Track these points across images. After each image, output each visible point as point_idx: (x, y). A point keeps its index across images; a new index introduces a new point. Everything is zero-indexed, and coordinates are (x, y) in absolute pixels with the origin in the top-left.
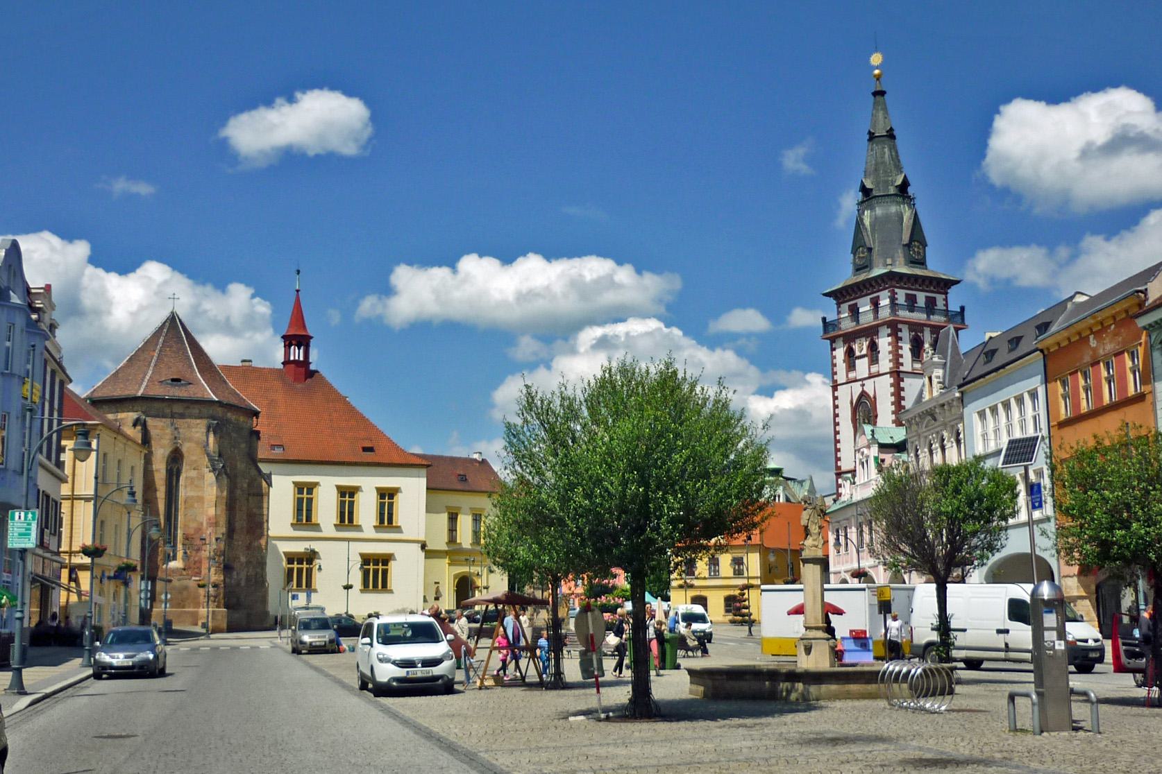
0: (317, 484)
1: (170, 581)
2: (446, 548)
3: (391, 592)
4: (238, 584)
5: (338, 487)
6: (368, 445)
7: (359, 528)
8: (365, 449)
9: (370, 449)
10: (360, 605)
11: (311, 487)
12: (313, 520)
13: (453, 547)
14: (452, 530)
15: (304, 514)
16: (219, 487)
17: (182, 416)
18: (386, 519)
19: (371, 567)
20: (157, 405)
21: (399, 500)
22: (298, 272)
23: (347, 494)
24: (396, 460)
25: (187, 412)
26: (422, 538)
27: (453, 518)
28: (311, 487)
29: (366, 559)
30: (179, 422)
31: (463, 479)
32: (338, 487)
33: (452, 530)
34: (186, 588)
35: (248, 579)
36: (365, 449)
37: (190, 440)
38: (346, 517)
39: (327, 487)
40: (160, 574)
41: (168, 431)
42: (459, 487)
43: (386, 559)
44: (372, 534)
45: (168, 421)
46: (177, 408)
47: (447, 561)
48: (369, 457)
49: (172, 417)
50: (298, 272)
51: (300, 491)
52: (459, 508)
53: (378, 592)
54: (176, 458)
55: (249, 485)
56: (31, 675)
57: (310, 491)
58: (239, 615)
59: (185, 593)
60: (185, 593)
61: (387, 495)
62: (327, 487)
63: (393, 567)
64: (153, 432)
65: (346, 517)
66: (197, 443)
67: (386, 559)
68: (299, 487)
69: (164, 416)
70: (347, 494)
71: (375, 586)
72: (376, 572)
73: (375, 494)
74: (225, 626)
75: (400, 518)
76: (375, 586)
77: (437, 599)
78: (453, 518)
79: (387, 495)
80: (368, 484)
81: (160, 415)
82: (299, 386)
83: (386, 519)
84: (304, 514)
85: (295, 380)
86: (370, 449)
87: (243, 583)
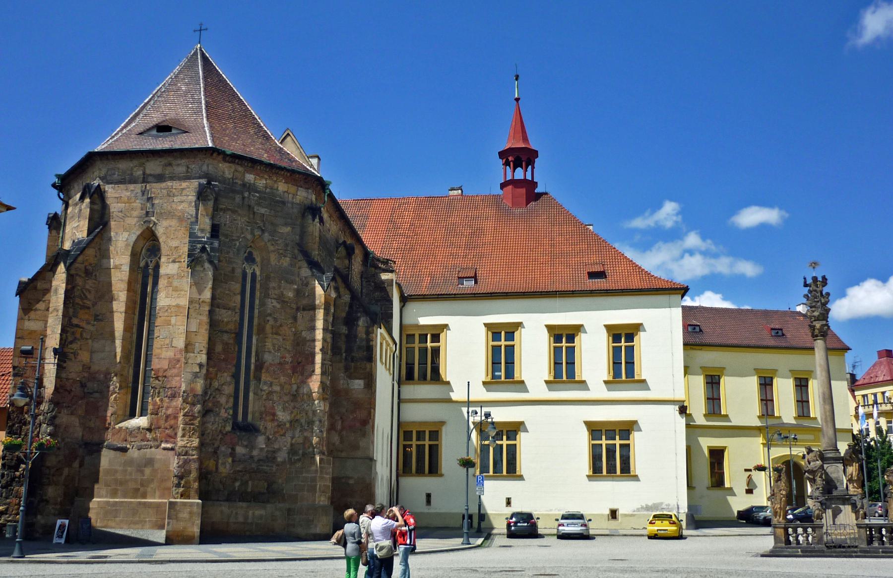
0: (519, 325)
1: (124, 450)
2: (757, 423)
3: (636, 478)
4: (270, 458)
5: (550, 328)
6: (597, 268)
7: (583, 385)
8: (592, 275)
9: (601, 275)
10: (598, 498)
11: (511, 331)
12: (517, 377)
13: (771, 421)
14: (767, 401)
15: (502, 363)
16: (198, 284)
17: (160, 178)
18: (623, 366)
19: (604, 442)
20: (123, 165)
21: (642, 342)
22: (517, 78)
23: (564, 337)
24: (636, 284)
25: (168, 170)
26: (680, 395)
27: (766, 384)
28: (511, 331)
29: (595, 429)
30: (155, 188)
31: (779, 333)
32: (550, 328)
33: (767, 401)
34: (150, 462)
35: (293, 451)
36: (592, 275)
37: (170, 215)
38: (564, 369)
39: (534, 328)
40: (110, 438)
41: (137, 204)
42: (772, 342)
43: (627, 429)
44: (603, 393)
45: (138, 188)
46: (154, 167)
47: (761, 440)
48: (599, 284)
49: (145, 181)
50: (517, 78)
51: (496, 336)
52: (775, 371)
53: (604, 478)
54: (148, 248)
55: (298, 292)
56: (471, 540)
57: (510, 336)
58: (222, 511)
59: (148, 471)
60: (148, 471)
61: (623, 337)
62: (534, 328)
63: (637, 440)
64: (114, 207)
65: (564, 369)
66: (181, 219)
67: (627, 429)
68: (494, 331)
69: (133, 181)
70: (564, 337)
71: (611, 470)
72: (611, 453)
73: (604, 335)
74: (196, 530)
75: (644, 368)
76: (611, 470)
77: (749, 491)
78: (766, 384)
79: (623, 337)
80: (595, 322)
81: (127, 180)
82: (517, 211)
83: (623, 366)
84: (502, 363)
85: (514, 204)
86: (601, 275)
87: (281, 456)
